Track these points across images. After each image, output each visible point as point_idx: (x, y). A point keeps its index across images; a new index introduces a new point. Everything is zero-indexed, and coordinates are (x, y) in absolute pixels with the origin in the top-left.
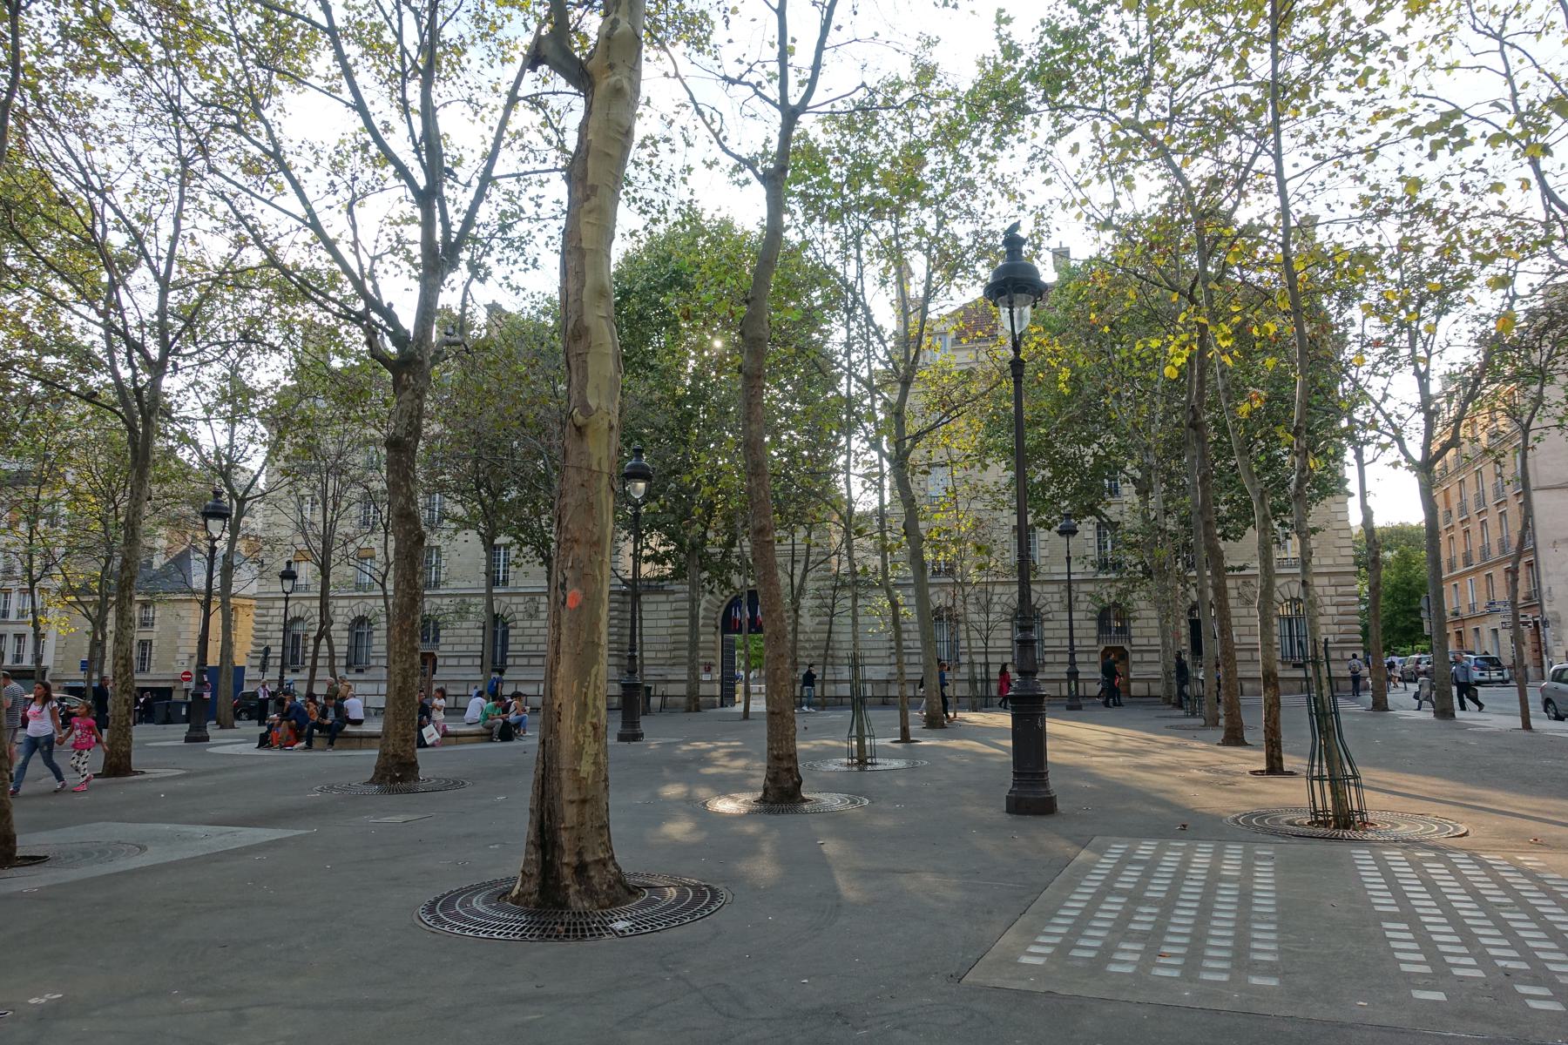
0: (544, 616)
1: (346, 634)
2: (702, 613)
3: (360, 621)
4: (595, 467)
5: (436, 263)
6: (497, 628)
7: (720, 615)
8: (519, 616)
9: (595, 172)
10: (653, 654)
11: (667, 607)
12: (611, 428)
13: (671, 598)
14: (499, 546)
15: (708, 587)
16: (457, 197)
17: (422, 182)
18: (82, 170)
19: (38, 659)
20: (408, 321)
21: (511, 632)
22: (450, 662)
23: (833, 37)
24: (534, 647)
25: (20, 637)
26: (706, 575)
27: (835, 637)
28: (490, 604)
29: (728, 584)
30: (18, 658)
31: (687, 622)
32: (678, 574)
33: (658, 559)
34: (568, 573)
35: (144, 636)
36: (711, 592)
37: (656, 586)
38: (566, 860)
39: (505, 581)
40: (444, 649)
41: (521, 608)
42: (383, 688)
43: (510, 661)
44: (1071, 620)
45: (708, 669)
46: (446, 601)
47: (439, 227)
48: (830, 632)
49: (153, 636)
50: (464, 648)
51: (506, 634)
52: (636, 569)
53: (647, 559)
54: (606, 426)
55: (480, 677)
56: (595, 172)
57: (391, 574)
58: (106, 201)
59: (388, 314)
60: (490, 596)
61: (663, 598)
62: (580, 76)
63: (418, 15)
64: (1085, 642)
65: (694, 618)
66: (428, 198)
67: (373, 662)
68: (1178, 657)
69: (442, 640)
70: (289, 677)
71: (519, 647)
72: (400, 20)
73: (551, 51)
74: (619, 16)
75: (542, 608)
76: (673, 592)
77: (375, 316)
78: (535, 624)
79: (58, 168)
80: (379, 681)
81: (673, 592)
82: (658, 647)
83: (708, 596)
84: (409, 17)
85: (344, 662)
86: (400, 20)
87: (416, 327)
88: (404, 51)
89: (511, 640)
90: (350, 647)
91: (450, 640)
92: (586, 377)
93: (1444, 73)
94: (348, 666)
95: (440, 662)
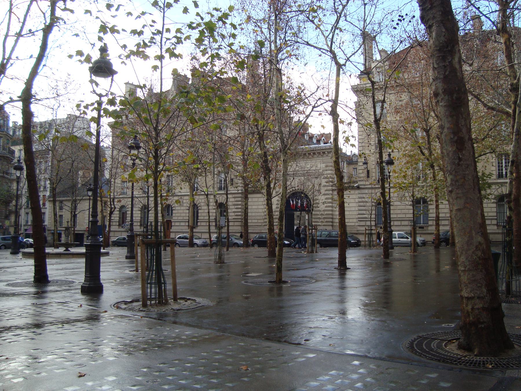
1: (139, 212)
3: (123, 207)
6: (195, 208)
19: (238, 233)
21: (200, 211)
22: (177, 224)
35: (61, 214)
40: (174, 218)
43: (199, 224)
44: (209, 209)
50: (182, 218)
51: (198, 213)
57: (41, 203)
64: (490, 214)
69: (174, 215)
82: (259, 218)
89: (199, 215)
90: (141, 218)
91: (177, 215)
93: (92, 90)
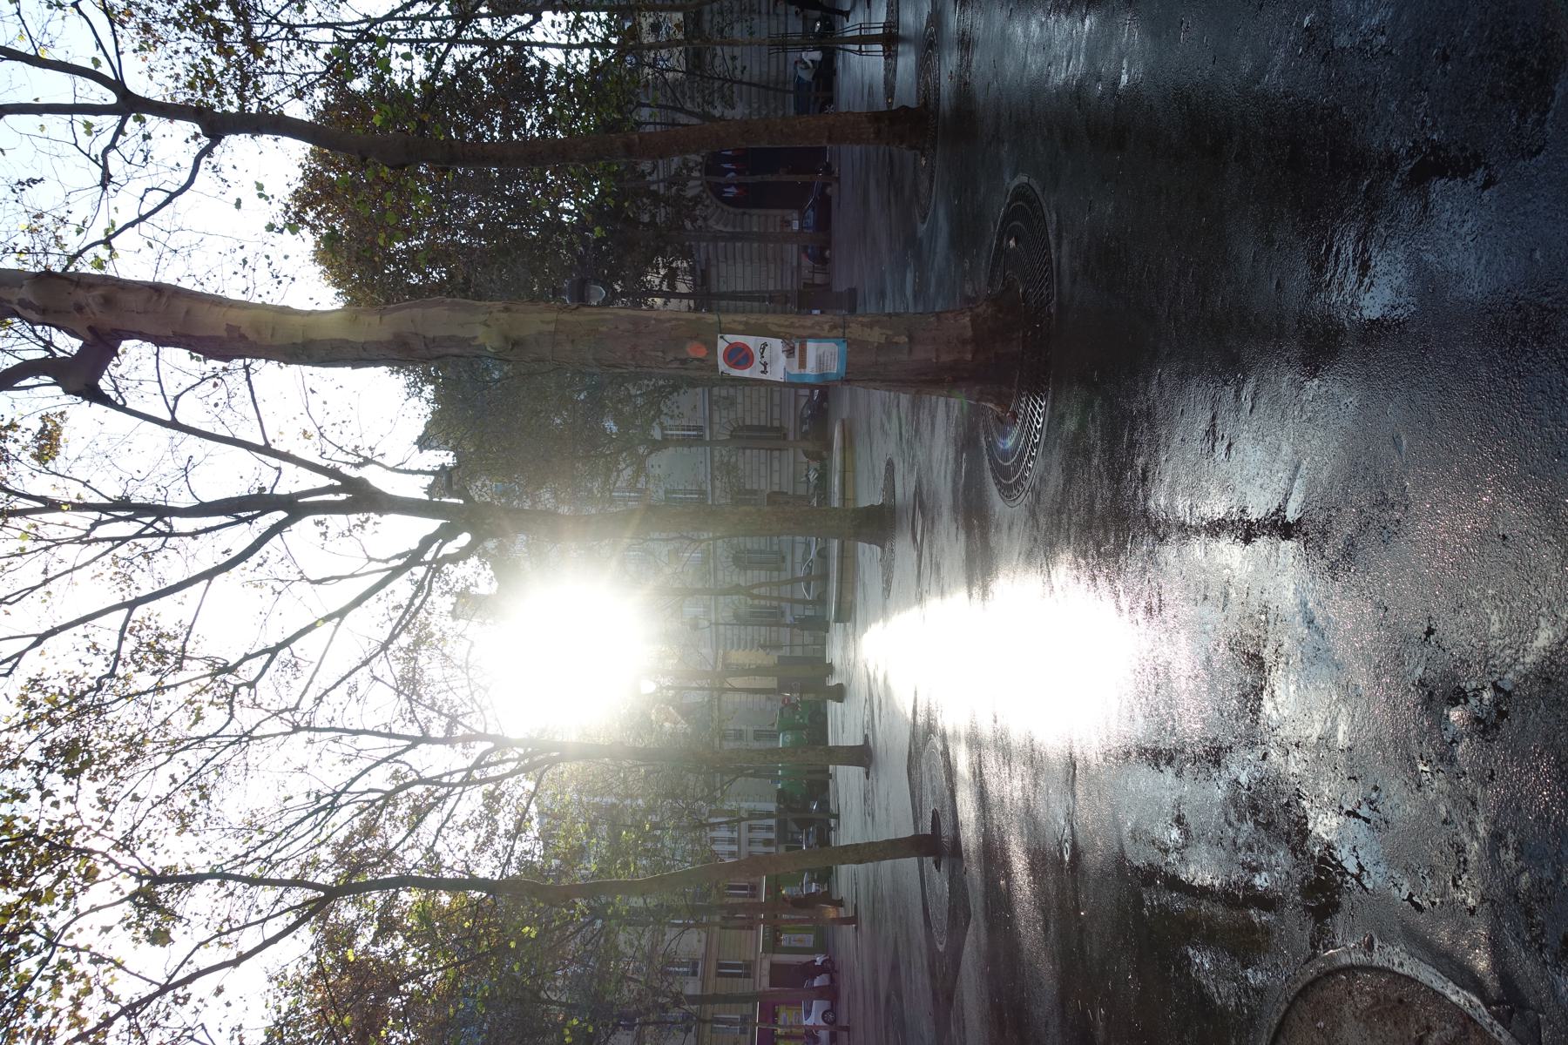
0: (732, 391)
2: (729, 229)
4: (552, 327)
5: (362, 499)
7: (731, 209)
8: (732, 415)
9: (222, 332)
10: (771, 282)
11: (723, 266)
12: (507, 310)
13: (714, 262)
14: (664, 436)
15: (700, 222)
16: (294, 481)
17: (281, 515)
18: (317, 812)
20: (431, 525)
21: (748, 422)
23: (24, 47)
24: (763, 401)
25: (751, 829)
26: (688, 224)
27: (755, 80)
28: (721, 443)
29: (696, 200)
30: (769, 828)
31: (739, 245)
32: (686, 254)
33: (672, 276)
34: (670, 357)
36: (705, 219)
37: (702, 278)
38: (969, 357)
39: (700, 428)
41: (724, 413)
42: (799, 539)
45: (789, 223)
46: (717, 483)
47: (330, 497)
48: (750, 84)
49: (751, 729)
52: (681, 296)
53: (672, 286)
54: (504, 315)
55: (791, 451)
56: (222, 332)
58: (344, 791)
59: (427, 542)
60: (713, 443)
61: (713, 271)
62: (101, 348)
63: (99, 522)
65: (734, 237)
66: (296, 508)
67: (775, 548)
68: (1060, 843)
69: (755, 487)
70: (789, 619)
71: (763, 415)
72: (103, 540)
73: (82, 378)
74: (14, 299)
75: (724, 393)
76: (708, 259)
77: (428, 557)
78: (740, 400)
79: (317, 830)
80: (793, 542)
81: (708, 259)
83: (711, 222)
84: (100, 532)
85: (775, 573)
86: (103, 540)
87: (435, 517)
88: (139, 535)
89: (756, 423)
92: (450, 338)
94: (778, 569)
95: (776, 488)
